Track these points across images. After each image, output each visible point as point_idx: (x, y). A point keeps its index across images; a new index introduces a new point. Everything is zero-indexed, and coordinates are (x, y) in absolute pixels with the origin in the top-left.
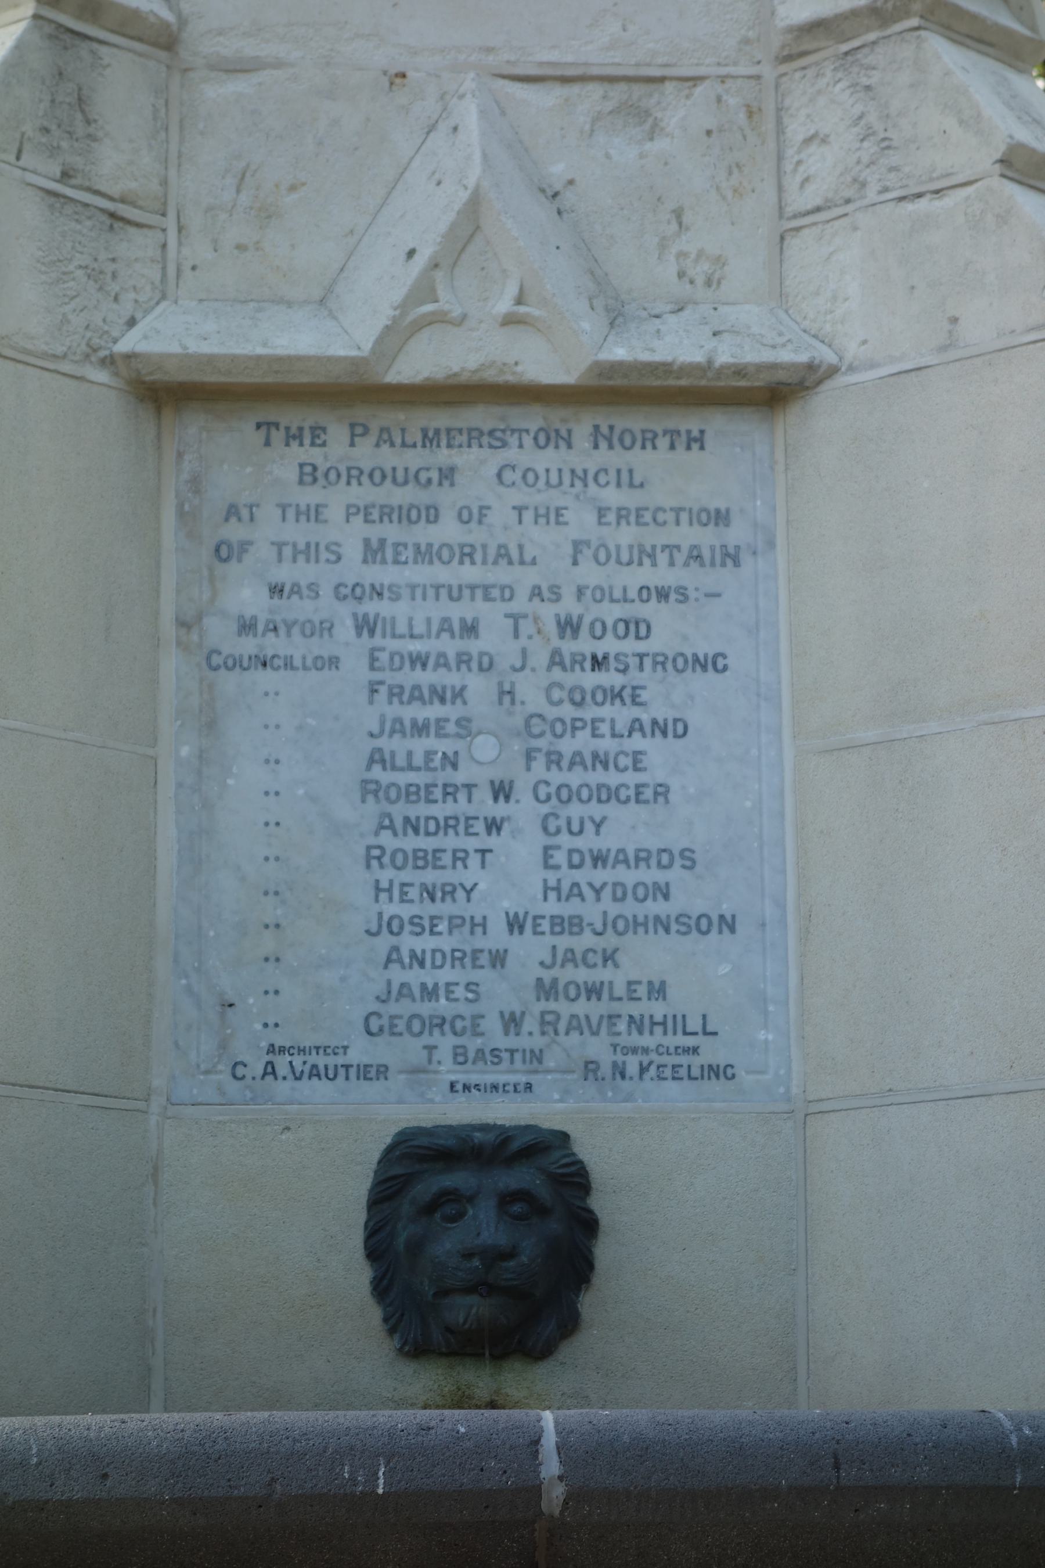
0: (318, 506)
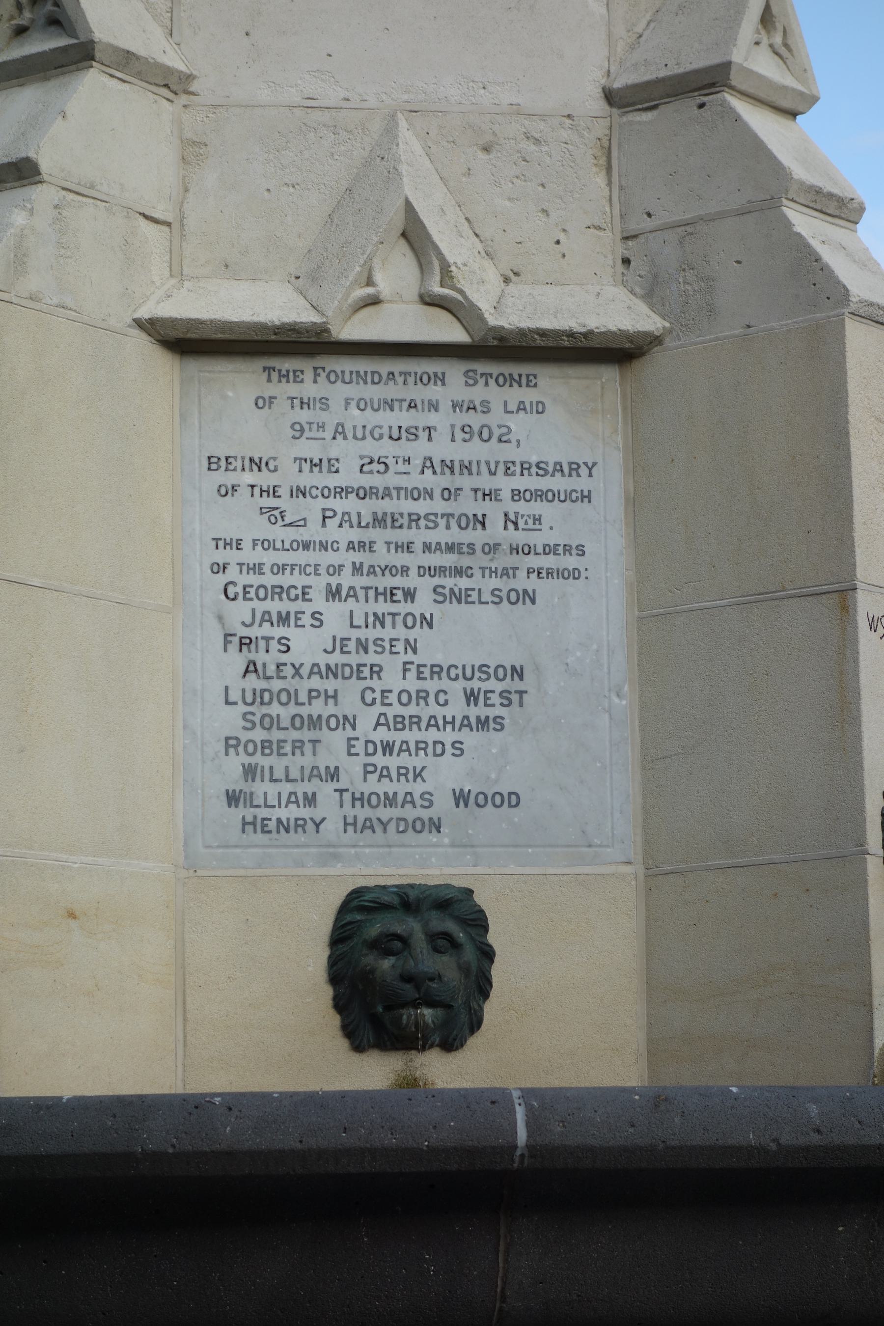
0: (274, 487)
